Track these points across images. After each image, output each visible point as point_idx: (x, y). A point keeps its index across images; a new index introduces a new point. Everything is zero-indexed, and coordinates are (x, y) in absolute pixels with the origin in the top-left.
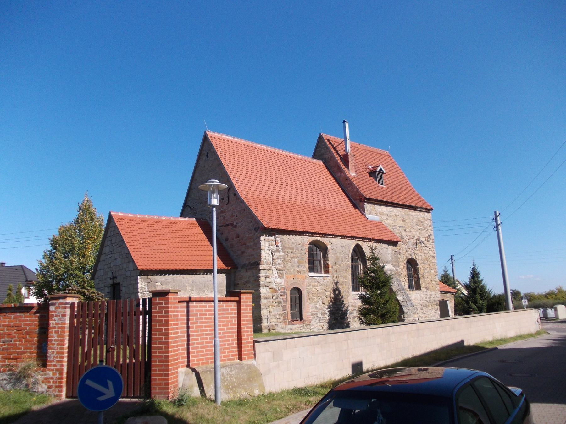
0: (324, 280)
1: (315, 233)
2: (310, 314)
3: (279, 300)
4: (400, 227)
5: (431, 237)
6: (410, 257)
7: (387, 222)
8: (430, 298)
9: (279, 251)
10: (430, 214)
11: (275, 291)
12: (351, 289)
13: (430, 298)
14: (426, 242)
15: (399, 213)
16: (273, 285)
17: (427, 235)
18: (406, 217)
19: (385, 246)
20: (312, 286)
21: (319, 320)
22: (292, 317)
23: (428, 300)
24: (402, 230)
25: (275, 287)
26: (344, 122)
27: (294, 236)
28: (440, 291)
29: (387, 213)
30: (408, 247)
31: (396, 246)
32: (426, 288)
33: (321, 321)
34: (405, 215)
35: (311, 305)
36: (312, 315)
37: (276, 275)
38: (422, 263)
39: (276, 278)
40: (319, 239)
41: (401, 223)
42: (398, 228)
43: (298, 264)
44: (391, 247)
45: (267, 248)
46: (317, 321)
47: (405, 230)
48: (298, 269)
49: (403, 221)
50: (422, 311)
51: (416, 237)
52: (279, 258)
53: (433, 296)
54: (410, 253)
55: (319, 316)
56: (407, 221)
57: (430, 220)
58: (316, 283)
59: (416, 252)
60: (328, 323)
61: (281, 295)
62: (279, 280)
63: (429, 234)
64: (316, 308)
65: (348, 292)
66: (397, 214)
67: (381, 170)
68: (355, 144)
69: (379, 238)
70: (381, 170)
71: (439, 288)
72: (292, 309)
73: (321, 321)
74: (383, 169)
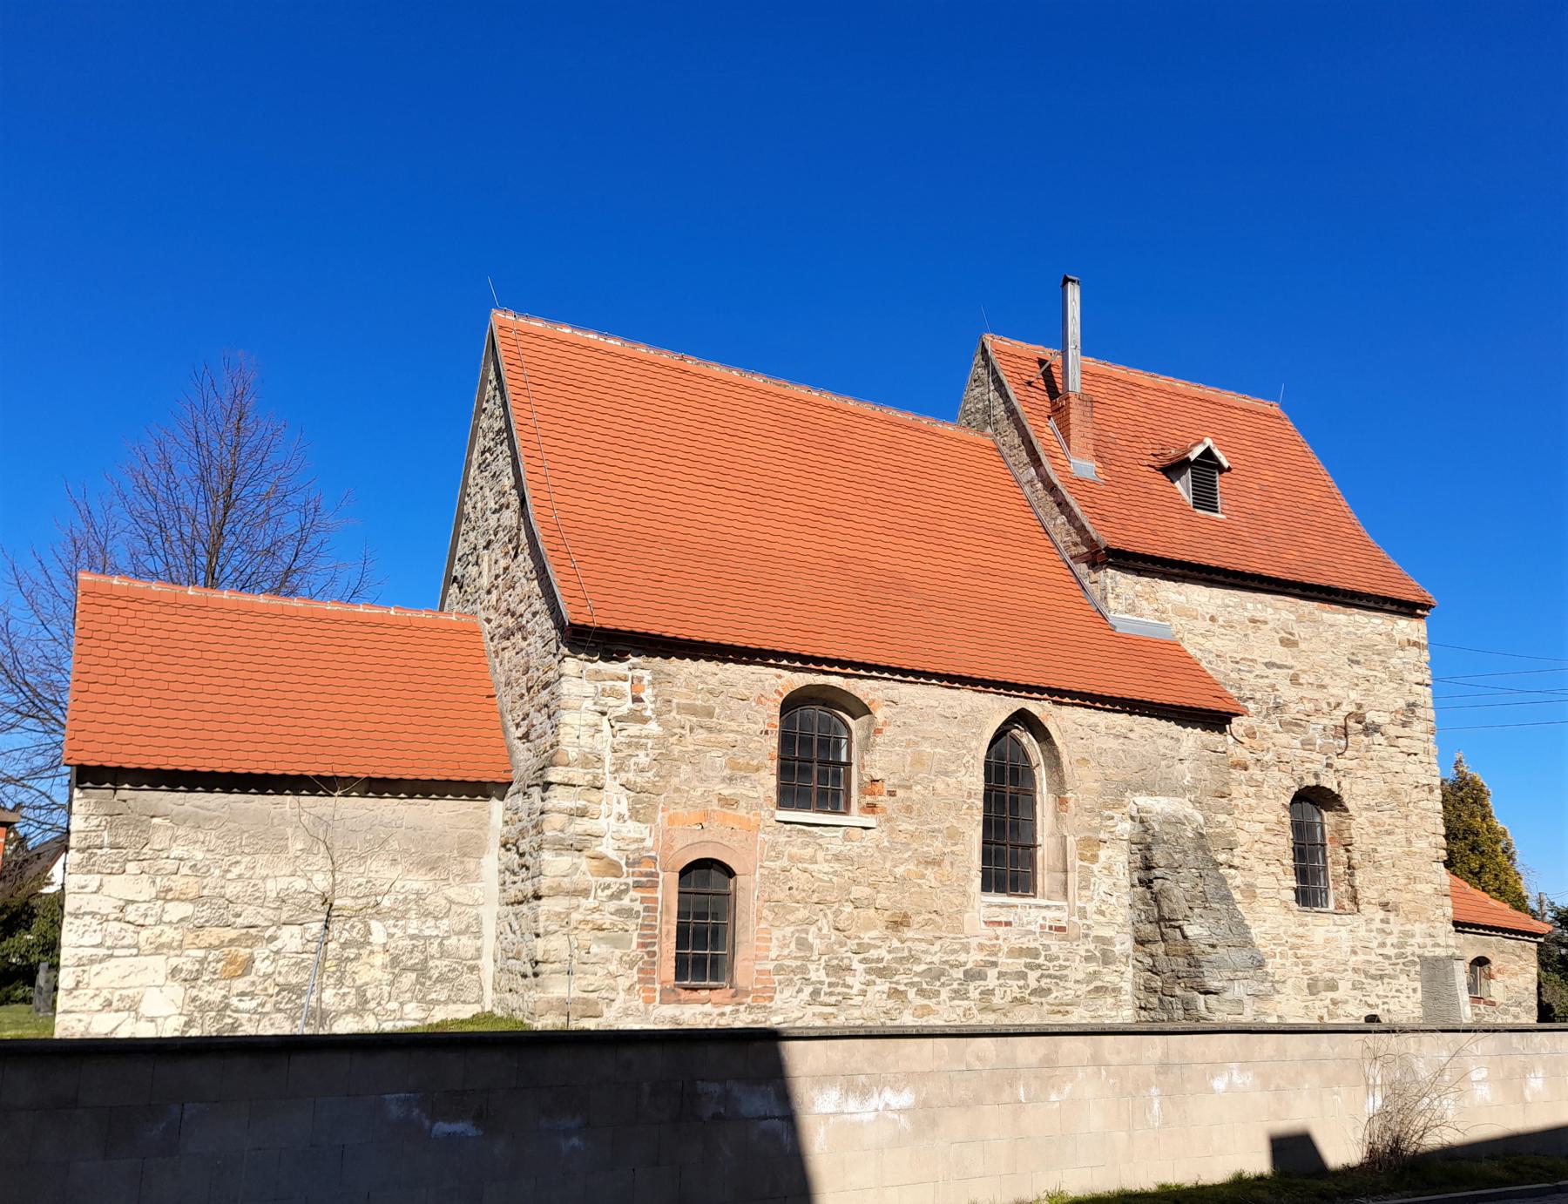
0: (847, 838)
1: (818, 661)
2: (770, 966)
3: (626, 902)
4: (1269, 665)
5: (1419, 712)
6: (1310, 781)
7: (1208, 645)
8: (1402, 945)
9: (645, 721)
10: (1415, 623)
11: (613, 868)
12: (978, 881)
13: (1402, 945)
14: (1393, 731)
15: (1269, 614)
16: (607, 848)
17: (1401, 703)
18: (1300, 631)
19: (1171, 728)
20: (791, 858)
21: (816, 993)
22: (680, 974)
23: (1391, 952)
24: (1280, 678)
25: (612, 855)
26: (1066, 280)
27: (711, 666)
28: (1456, 924)
29: (1212, 611)
30: (1307, 744)
31: (1222, 731)
32: (1384, 906)
33: (823, 998)
34: (1299, 621)
35: (776, 933)
36: (779, 969)
37: (624, 808)
38: (1368, 808)
39: (620, 817)
40: (835, 681)
41: (1280, 654)
42: (1260, 669)
43: (727, 772)
44: (1192, 738)
45: (588, 703)
46: (805, 995)
47: (1294, 680)
48: (726, 792)
49: (1287, 643)
50: (1358, 994)
51: (1347, 708)
52: (639, 746)
53: (1418, 940)
54: (1318, 767)
55: (813, 976)
56: (1303, 646)
57: (1416, 644)
58: (810, 851)
59: (1339, 763)
60: (1371, 1152)
61: (637, 885)
62: (632, 829)
63: (1412, 700)
64: (802, 944)
65: (964, 894)
66: (1259, 616)
67: (1208, 453)
68: (1091, 363)
69: (1128, 694)
70: (1208, 453)
71: (1449, 911)
72: (680, 944)
73: (823, 998)
74: (1217, 452)
